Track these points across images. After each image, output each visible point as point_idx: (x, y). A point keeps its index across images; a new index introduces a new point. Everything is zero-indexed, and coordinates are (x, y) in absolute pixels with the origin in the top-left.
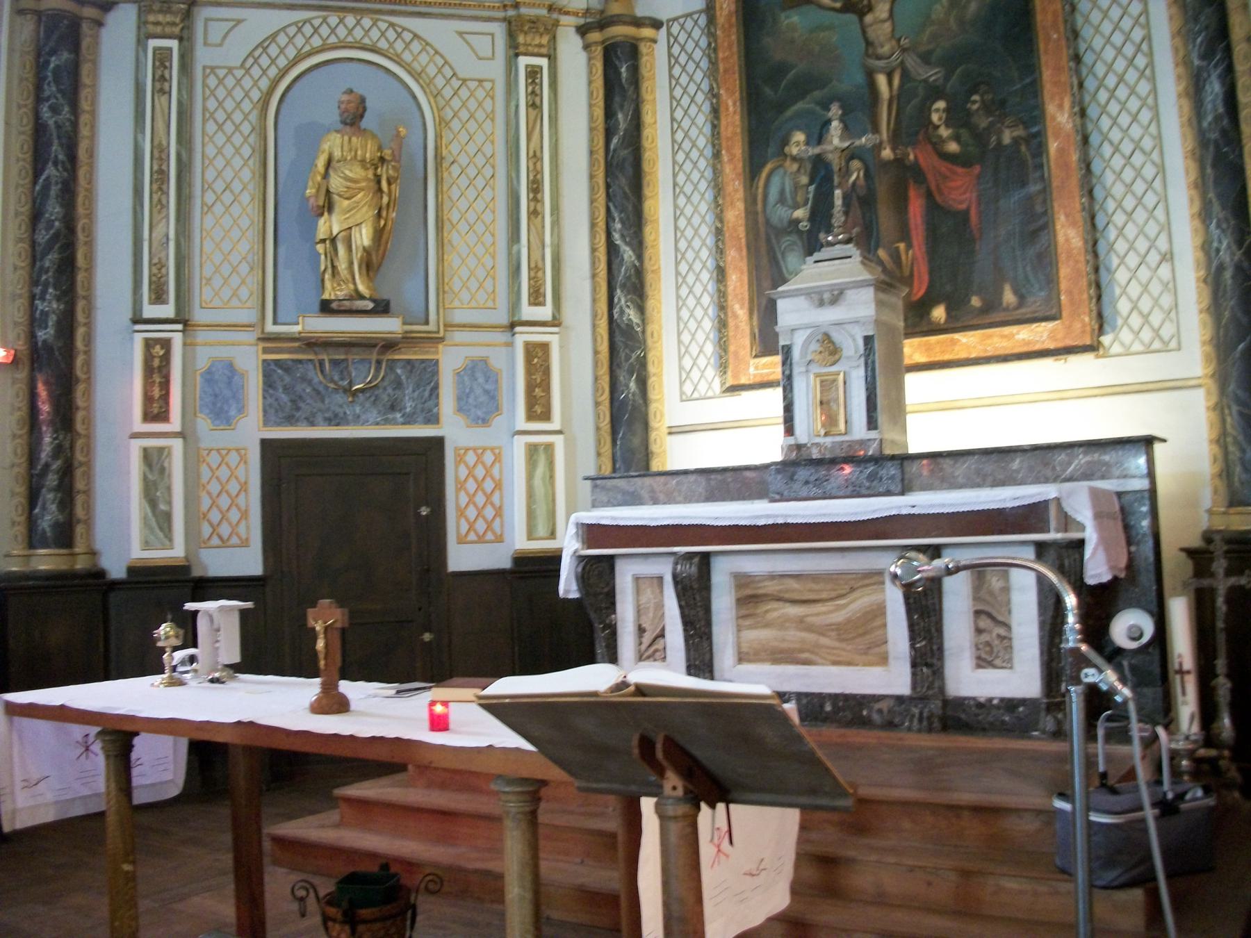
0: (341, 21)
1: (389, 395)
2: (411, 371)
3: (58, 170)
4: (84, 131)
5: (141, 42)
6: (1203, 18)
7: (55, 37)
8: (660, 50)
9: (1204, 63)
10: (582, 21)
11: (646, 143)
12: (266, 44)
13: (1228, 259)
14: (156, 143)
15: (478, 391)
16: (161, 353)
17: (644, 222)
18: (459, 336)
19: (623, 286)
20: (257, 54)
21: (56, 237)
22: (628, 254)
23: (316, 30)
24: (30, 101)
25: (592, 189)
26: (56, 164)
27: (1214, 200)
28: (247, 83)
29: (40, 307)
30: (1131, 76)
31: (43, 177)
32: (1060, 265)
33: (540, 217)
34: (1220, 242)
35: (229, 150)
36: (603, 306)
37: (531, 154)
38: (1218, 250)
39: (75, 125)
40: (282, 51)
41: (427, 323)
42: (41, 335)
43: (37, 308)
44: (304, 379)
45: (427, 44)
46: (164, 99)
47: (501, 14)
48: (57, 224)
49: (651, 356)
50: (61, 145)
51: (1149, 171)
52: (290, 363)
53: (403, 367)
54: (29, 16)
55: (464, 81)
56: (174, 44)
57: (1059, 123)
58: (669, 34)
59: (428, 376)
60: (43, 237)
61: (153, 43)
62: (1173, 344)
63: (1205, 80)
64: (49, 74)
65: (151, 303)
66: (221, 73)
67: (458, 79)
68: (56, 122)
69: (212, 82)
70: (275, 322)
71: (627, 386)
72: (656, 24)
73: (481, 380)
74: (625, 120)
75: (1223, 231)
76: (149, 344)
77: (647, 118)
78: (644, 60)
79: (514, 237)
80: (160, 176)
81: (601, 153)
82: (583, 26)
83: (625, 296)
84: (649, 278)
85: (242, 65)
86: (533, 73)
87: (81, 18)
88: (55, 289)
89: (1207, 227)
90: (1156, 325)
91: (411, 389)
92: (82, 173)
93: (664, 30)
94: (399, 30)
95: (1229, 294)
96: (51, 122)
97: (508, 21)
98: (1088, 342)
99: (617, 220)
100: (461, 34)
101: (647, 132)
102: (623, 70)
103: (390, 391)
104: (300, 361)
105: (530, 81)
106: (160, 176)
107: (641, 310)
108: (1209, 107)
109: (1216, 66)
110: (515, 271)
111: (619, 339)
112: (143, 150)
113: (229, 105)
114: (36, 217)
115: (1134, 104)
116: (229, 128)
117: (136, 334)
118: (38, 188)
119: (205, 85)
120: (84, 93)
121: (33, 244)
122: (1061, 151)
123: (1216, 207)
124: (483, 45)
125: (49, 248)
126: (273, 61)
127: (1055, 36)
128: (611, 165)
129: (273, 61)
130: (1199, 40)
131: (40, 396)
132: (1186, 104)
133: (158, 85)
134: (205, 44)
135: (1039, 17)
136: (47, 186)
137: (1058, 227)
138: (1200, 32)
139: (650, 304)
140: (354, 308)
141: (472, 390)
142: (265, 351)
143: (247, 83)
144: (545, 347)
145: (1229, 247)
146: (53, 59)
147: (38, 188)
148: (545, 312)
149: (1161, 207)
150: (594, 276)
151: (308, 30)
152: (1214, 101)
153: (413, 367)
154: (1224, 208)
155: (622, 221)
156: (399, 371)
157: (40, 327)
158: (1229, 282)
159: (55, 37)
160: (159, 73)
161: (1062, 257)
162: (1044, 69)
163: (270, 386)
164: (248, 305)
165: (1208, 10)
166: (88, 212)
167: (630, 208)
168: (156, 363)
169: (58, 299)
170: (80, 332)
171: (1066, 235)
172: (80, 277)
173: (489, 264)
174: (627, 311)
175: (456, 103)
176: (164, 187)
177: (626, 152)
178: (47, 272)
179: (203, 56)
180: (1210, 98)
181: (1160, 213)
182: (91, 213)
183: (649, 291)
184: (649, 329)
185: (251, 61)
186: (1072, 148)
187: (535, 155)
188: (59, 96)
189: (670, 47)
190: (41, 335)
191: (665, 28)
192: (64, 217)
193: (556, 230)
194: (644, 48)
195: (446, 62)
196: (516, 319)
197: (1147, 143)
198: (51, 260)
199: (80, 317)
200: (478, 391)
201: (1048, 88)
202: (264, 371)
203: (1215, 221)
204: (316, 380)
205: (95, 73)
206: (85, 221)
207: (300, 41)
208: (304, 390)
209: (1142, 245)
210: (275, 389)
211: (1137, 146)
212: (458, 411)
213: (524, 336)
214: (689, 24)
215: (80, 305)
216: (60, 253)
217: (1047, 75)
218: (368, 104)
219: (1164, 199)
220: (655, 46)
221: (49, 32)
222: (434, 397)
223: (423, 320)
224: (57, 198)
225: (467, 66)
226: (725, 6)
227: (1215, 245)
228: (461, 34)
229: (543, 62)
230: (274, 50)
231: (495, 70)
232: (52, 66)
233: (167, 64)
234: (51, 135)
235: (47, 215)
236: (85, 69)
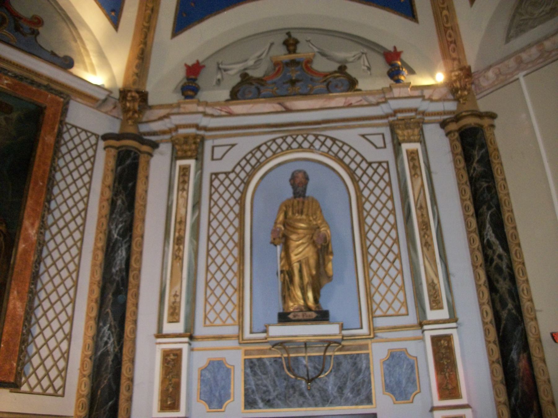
6: (125, 216)
9: (121, 239)
13: (112, 350)
27: (110, 313)
30: (72, 226)
32: (6, 322)
34: (109, 338)
38: (106, 343)
51: (69, 283)
55: (370, 164)
57: (29, 234)
62: (60, 392)
63: (119, 248)
75: (112, 333)
89: (99, 330)
90: (52, 378)
95: (109, 371)
98: (12, 380)
100: (363, 136)
108: (118, 262)
109: (126, 243)
115: (70, 242)
122: (25, 251)
123: (110, 318)
127: (41, 184)
130: (120, 226)
132: (101, 256)
134: (213, 159)
135: (35, 168)
137: (11, 298)
138: (122, 222)
144: (448, 338)
145: (114, 342)
149: (71, 306)
152: (121, 260)
154: (115, 320)
158: (110, 363)
161: (8, 319)
162: (29, 198)
165: (128, 213)
171: (14, 304)
180: (119, 258)
181: (69, 309)
186: (32, 253)
193: (170, 203)
197: (72, 267)
201: (28, 211)
203: (108, 325)
209: (55, 325)
211: (66, 266)
212: (407, 398)
213: (430, 332)
217: (30, 202)
219: (73, 301)
223: (359, 326)
225: (372, 155)
227: (105, 339)
228: (363, 136)
231: (387, 155)
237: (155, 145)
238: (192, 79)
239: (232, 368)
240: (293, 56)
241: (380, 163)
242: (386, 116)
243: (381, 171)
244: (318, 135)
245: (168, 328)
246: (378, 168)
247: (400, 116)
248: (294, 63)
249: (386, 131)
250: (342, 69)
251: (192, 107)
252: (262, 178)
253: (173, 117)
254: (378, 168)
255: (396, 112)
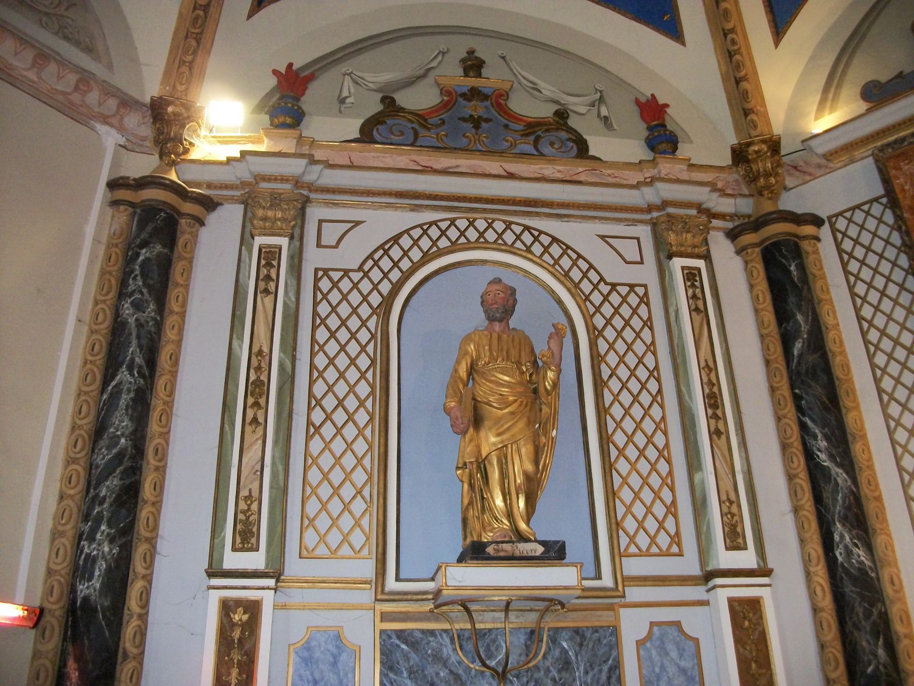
0: (471, 223)
1: (554, 680)
2: (581, 645)
3: (132, 375)
4: (170, 334)
5: (245, 240)
7: (149, 228)
8: (827, 250)
10: (730, 225)
11: (831, 346)
12: (387, 247)
14: (255, 349)
15: (672, 670)
16: (245, 617)
17: (850, 438)
18: (634, 594)
19: (844, 520)
20: (376, 257)
21: (120, 456)
22: (840, 475)
23: (443, 233)
24: (113, 294)
25: (777, 404)
26: (130, 369)
28: (365, 286)
29: (86, 550)
31: (114, 383)
33: (723, 437)
35: (342, 361)
36: (816, 548)
37: (703, 364)
39: (159, 325)
40: (406, 253)
41: (598, 577)
42: (83, 589)
43: (82, 552)
44: (437, 657)
45: (568, 247)
46: (269, 300)
47: (648, 217)
48: (123, 440)
49: (894, 612)
50: (140, 346)
52: (418, 635)
53: (571, 639)
54: (122, 208)
55: (614, 286)
56: (284, 242)
58: (834, 231)
59: (601, 652)
60: (103, 457)
61: (259, 241)
64: (137, 267)
65: (234, 549)
66: (336, 276)
67: (606, 284)
68: (137, 320)
69: (325, 284)
70: (398, 579)
71: (875, 655)
72: (817, 221)
73: (674, 654)
74: (806, 322)
76: (227, 607)
77: (827, 319)
78: (810, 260)
79: (693, 464)
80: (257, 389)
81: (781, 364)
82: (732, 230)
83: (850, 531)
84: (870, 508)
85: (360, 268)
86: (691, 275)
87: (181, 215)
88: (110, 526)
91: (582, 669)
92: (161, 383)
93: (826, 228)
94: (536, 233)
96: (132, 320)
97: (654, 224)
99: (820, 436)
100: (603, 237)
101: (830, 336)
102: (793, 268)
103: (554, 673)
104: (432, 633)
105: (689, 284)
106: (257, 389)
107: (869, 548)
110: (699, 507)
111: (849, 589)
112: (239, 359)
113: (344, 310)
114: (99, 430)
116: (343, 335)
117: (211, 591)
118: (105, 397)
119: (316, 288)
120: (173, 293)
121: (91, 466)
124: (630, 250)
125: (108, 471)
126: (396, 264)
128: (799, 374)
129: (396, 264)
131: (69, 678)
133: (262, 285)
134: (319, 245)
136: (116, 395)
139: (879, 541)
140: (517, 553)
141: (663, 668)
142: (385, 617)
143: (365, 286)
144: (755, 604)
146: (144, 251)
147: (105, 397)
148: (747, 559)
150: (796, 510)
151: (434, 232)
153: (583, 637)
155: (826, 437)
156: (565, 645)
157: (82, 577)
159: (149, 228)
160: (264, 271)
163: (391, 668)
164: (365, 552)
166: (165, 430)
167: (833, 422)
168: (237, 634)
169: (112, 541)
170: (135, 590)
172: (144, 513)
173: (668, 499)
174: (856, 550)
175: (607, 310)
176: (262, 401)
177: (815, 356)
178: (101, 503)
179: (314, 258)
182: (169, 432)
183: (873, 522)
184: (885, 575)
185: (370, 263)
187: (707, 366)
188: (145, 291)
189: (838, 245)
190: (83, 589)
191: (827, 225)
192: (134, 433)
194: (806, 245)
195: (591, 266)
196: (709, 568)
198: (111, 486)
199: (138, 565)
200: (672, 670)
202: (382, 646)
204: (453, 659)
205: (188, 272)
206: (157, 441)
207: (425, 243)
208: (437, 674)
210: (398, 672)
214: (876, 209)
215: (140, 550)
216: (121, 479)
218: (518, 296)
220: (819, 245)
221: (142, 225)
222: (613, 680)
223: (592, 575)
224: (127, 410)
225: (615, 271)
226: (907, 188)
228: (603, 237)
229: (700, 264)
230: (396, 253)
231: (647, 274)
232: (141, 258)
233: (275, 263)
234: (130, 334)
235: (112, 430)
236: (177, 269)
237: (210, 205)
238: (657, 126)
239: (292, 648)
240: (472, 82)
241: (632, 287)
242: (650, 208)
243: (633, 300)
244: (511, 223)
245: (232, 560)
246: (628, 294)
247: (671, 210)
248: (474, 94)
249: (644, 232)
250: (562, 115)
251: (666, 167)
252: (552, 293)
253: (659, 185)
254: (628, 294)
255: (665, 204)
